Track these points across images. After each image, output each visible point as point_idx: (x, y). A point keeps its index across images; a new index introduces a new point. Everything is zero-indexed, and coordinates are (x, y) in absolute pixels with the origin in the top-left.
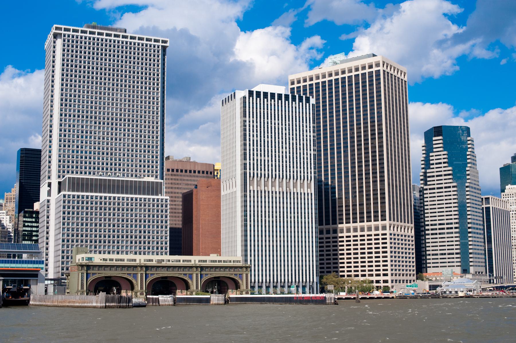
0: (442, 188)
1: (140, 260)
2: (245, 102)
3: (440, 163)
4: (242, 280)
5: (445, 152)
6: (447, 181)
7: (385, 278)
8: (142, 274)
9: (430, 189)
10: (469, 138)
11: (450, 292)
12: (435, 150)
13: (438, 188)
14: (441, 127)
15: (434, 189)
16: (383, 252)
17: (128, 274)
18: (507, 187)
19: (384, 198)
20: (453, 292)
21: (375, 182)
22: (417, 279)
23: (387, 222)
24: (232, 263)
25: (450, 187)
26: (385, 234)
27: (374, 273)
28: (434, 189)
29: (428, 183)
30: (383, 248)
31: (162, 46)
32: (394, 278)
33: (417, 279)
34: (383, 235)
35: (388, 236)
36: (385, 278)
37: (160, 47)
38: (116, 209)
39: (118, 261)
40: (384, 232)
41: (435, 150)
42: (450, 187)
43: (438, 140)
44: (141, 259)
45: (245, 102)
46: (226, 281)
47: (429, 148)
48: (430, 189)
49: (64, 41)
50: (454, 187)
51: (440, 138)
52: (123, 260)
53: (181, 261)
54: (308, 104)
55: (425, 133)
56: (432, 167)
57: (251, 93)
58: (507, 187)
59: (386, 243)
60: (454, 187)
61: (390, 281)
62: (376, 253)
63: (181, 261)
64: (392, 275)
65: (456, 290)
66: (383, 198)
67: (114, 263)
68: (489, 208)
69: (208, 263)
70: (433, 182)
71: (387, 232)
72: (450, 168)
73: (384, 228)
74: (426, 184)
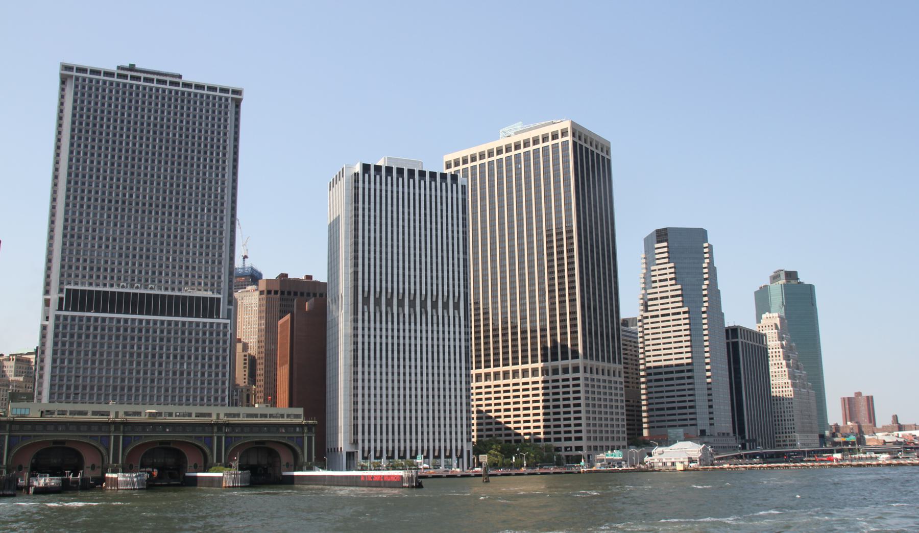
0: (663, 315)
1: (218, 415)
2: (356, 181)
3: (666, 280)
4: (211, 449)
5: (672, 265)
6: (674, 304)
7: (579, 443)
8: (219, 439)
9: (652, 317)
10: (705, 245)
11: (664, 464)
12: (658, 262)
13: (663, 315)
14: (666, 229)
15: (657, 316)
16: (575, 405)
17: (289, 437)
18: (764, 316)
19: (576, 325)
20: (669, 464)
21: (562, 302)
22: (629, 445)
23: (580, 362)
24: (285, 419)
25: (679, 313)
26: (578, 379)
27: (563, 436)
28: (657, 316)
29: (650, 308)
30: (575, 399)
31: (233, 99)
32: (592, 443)
33: (629, 445)
34: (574, 379)
35: (581, 382)
36: (579, 443)
37: (230, 101)
38: (165, 340)
39: (276, 417)
40: (576, 375)
41: (658, 262)
42: (679, 313)
43: (661, 248)
44: (116, 411)
45: (356, 181)
46: (276, 448)
47: (650, 260)
48: (652, 317)
49: (76, 86)
50: (684, 313)
51: (665, 244)
52: (85, 413)
53: (194, 415)
54: (454, 186)
55: (645, 239)
56: (654, 285)
57: (366, 168)
58: (764, 316)
59: (579, 392)
60: (684, 313)
61: (585, 448)
62: (565, 406)
63: (194, 415)
64: (589, 439)
65: (673, 460)
66: (574, 326)
67: (68, 418)
68: (737, 343)
69: (241, 418)
70: (657, 307)
71: (581, 375)
72: (679, 287)
73: (576, 369)
74: (647, 311)
